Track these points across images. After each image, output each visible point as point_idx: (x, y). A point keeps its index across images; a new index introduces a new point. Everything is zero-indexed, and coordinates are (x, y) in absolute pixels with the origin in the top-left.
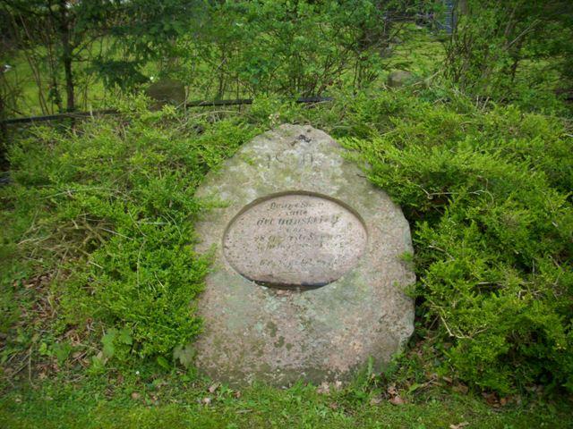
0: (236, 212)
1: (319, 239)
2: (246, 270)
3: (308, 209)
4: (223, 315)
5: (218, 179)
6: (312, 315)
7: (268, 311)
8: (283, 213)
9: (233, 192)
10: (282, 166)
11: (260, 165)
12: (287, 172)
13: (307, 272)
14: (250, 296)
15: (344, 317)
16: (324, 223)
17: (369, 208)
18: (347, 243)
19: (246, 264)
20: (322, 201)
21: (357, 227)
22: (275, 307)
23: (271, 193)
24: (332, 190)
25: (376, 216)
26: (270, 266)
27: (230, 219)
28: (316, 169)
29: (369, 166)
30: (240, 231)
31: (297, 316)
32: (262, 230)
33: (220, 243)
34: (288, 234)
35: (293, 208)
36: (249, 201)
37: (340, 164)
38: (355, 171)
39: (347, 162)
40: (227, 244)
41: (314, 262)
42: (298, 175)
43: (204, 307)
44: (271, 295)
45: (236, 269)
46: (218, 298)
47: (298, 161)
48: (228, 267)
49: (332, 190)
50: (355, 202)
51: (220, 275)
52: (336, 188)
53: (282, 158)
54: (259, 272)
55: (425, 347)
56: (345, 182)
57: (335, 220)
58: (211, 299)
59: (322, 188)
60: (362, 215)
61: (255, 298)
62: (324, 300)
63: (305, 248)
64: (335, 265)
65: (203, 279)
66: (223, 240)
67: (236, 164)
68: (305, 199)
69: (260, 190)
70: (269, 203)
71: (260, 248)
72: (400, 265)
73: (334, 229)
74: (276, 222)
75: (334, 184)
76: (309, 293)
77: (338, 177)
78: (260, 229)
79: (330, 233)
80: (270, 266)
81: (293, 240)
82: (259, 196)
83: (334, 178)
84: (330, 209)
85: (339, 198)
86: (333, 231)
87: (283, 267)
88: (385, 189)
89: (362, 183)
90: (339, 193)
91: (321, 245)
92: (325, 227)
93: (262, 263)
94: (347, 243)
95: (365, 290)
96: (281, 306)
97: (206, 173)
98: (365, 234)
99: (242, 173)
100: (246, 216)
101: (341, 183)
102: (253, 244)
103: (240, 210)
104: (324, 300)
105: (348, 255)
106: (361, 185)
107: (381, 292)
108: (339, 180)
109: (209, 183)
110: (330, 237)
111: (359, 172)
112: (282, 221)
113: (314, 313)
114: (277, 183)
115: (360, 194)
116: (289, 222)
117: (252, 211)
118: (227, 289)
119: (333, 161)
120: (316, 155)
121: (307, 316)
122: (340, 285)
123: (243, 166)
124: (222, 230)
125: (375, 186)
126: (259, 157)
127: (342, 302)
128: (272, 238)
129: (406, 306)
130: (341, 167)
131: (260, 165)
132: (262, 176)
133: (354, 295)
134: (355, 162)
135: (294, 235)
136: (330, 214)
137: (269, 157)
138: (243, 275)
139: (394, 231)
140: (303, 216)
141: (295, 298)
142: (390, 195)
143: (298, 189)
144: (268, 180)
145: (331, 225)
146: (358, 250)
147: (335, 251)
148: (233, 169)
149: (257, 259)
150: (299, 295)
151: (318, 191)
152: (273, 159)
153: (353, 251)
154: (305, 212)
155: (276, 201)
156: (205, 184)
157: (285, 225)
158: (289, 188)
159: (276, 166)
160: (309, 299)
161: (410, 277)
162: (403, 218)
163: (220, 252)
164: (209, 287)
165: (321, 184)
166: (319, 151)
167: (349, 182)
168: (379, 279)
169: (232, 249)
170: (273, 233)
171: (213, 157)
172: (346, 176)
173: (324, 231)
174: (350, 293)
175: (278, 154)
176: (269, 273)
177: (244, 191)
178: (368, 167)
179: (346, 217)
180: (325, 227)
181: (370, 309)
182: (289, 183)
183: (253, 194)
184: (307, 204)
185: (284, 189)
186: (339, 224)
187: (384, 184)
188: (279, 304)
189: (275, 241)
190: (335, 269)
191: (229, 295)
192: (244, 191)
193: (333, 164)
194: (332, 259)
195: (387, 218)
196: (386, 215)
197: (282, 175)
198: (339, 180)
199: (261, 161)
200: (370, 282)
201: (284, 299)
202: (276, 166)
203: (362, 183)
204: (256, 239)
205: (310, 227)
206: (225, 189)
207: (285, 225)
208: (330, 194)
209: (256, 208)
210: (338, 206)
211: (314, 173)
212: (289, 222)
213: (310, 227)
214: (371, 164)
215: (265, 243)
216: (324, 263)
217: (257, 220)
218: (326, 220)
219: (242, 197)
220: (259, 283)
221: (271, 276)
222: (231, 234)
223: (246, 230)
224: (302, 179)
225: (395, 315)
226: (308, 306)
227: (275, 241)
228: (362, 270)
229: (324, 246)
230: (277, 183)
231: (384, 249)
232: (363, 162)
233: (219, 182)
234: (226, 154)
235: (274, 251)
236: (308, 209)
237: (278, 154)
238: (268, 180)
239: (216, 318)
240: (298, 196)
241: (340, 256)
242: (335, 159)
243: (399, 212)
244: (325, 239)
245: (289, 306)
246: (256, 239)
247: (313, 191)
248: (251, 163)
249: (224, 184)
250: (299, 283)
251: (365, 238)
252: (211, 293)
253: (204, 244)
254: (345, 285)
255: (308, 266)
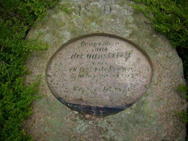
0: (55, 50)
1: (116, 71)
2: (63, 95)
3: (108, 47)
4: (46, 133)
5: (44, 24)
6: (112, 135)
7: (79, 132)
8: (90, 49)
9: (53, 34)
10: (89, 14)
11: (73, 13)
12: (93, 19)
13: (108, 97)
14: (65, 119)
15: (136, 137)
16: (120, 58)
17: (154, 48)
18: (137, 75)
19: (63, 90)
20: (118, 41)
21: (144, 62)
22: (84, 129)
23: (81, 35)
24: (125, 33)
25: (159, 55)
26: (81, 92)
27: (51, 55)
28: (113, 16)
29: (153, 15)
30: (59, 63)
31: (101, 136)
32: (75, 63)
33: (44, 74)
34: (94, 67)
35: (98, 46)
36: (65, 41)
37: (132, 13)
38: (143, 19)
39: (136, 12)
40: (50, 74)
41: (113, 89)
42: (101, 21)
43: (32, 125)
44: (81, 119)
45: (56, 95)
46: (42, 119)
47: (101, 11)
48: (49, 94)
49: (125, 33)
50: (143, 43)
51: (43, 100)
52: (128, 32)
53: (89, 8)
54: (72, 96)
55: (169, 30)
56: (136, 27)
57: (128, 55)
58: (37, 120)
59: (119, 31)
60: (148, 54)
61: (69, 120)
62: (121, 123)
63: (106, 77)
64: (128, 92)
65: (31, 105)
66: (47, 71)
67: (56, 13)
68: (106, 39)
69: (73, 32)
70: (80, 41)
71: (73, 77)
72: (176, 94)
73: (127, 63)
74: (84, 57)
75: (128, 28)
76: (110, 117)
77: (130, 24)
78: (74, 62)
79: (124, 66)
80: (81, 92)
81: (97, 71)
82: (72, 37)
83: (127, 23)
84: (124, 47)
85: (131, 39)
86: (127, 64)
87: (90, 93)
88: (167, 36)
89: (148, 29)
90: (131, 35)
91: (118, 76)
92: (121, 62)
93: (75, 89)
94: (137, 75)
95: (152, 115)
96: (88, 128)
97: (35, 20)
98: (150, 68)
99: (60, 20)
100: (64, 52)
101: (132, 28)
102: (68, 74)
103: (58, 48)
104: (121, 123)
105: (138, 84)
106: (147, 30)
107: (164, 116)
108: (131, 26)
109: (37, 27)
110: (124, 69)
111: (146, 20)
112: (89, 56)
113: (113, 134)
114: (85, 27)
115: (146, 37)
116: (94, 57)
117: (68, 48)
118: (49, 112)
119: (126, 11)
120: (113, 6)
121: (108, 137)
122: (134, 111)
123: (62, 14)
124: (46, 64)
125: (158, 32)
126: (73, 7)
127: (134, 125)
128: (82, 70)
129: (181, 127)
130: (133, 16)
131: (73, 13)
132: (75, 22)
133: (144, 120)
134: (143, 12)
135: (99, 67)
136: (124, 51)
137: (80, 7)
138: (59, 99)
139: (172, 67)
140: (105, 52)
141: (99, 122)
142: (169, 39)
143: (101, 31)
144: (79, 25)
145: (124, 59)
146: (144, 80)
147: (128, 81)
148: (54, 16)
149: (71, 86)
150: (102, 119)
151: (115, 34)
152: (83, 9)
153: (142, 80)
154: (106, 49)
155: (87, 40)
156: (35, 28)
157: (91, 58)
158: (94, 31)
159: (85, 14)
160: (109, 123)
161: (183, 104)
162: (178, 58)
163: (44, 81)
164: (36, 110)
165: (117, 28)
166: (116, 3)
167: (138, 27)
168: (162, 107)
169: (53, 77)
170: (82, 65)
171: (39, 7)
172: (135, 22)
173: (120, 65)
174: (140, 118)
175: (86, 5)
176: (80, 98)
177: (61, 33)
178: (152, 16)
179: (135, 54)
180: (121, 61)
181: (155, 131)
182: (94, 27)
183: (68, 36)
184: (107, 43)
185: (90, 32)
186: (131, 59)
187: (167, 30)
188: (86, 126)
189: (84, 72)
190: (128, 95)
191: (50, 118)
192: (61, 33)
193: (126, 13)
194: (126, 87)
195: (167, 57)
196: (166, 54)
197: (89, 21)
198: (131, 26)
199: (74, 10)
200: (155, 108)
201: (91, 122)
202: (85, 14)
203: (148, 29)
204: (70, 70)
205: (109, 61)
206: (48, 32)
207: (91, 58)
208: (125, 36)
209: (71, 45)
210: (130, 45)
211: (112, 20)
212: (94, 57)
213: (109, 61)
214: (154, 14)
215: (77, 73)
216: (120, 89)
217: (71, 55)
218: (121, 56)
219: (61, 38)
220: (73, 107)
221: (81, 100)
222: (53, 65)
223: (63, 62)
224: (104, 24)
225: (174, 135)
226: (109, 128)
227: (84, 72)
228: (149, 98)
229: (120, 76)
230: (85, 27)
231: (166, 82)
232: (149, 12)
233: (45, 26)
234: (49, 5)
235: (84, 79)
236: (108, 47)
237: (86, 5)
238: (79, 25)
239: (40, 134)
240: (101, 37)
241: (131, 84)
242: (127, 9)
243: (175, 52)
244: (121, 71)
245: (95, 128)
246: (70, 70)
247: (112, 33)
248: (67, 12)
249: (48, 28)
250: (102, 106)
251: (150, 71)
252: (37, 114)
253: (33, 74)
254: (137, 112)
255: (109, 92)
